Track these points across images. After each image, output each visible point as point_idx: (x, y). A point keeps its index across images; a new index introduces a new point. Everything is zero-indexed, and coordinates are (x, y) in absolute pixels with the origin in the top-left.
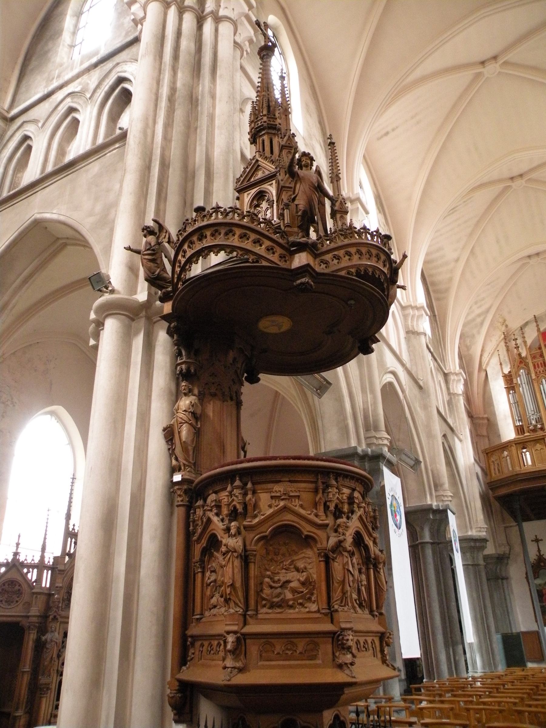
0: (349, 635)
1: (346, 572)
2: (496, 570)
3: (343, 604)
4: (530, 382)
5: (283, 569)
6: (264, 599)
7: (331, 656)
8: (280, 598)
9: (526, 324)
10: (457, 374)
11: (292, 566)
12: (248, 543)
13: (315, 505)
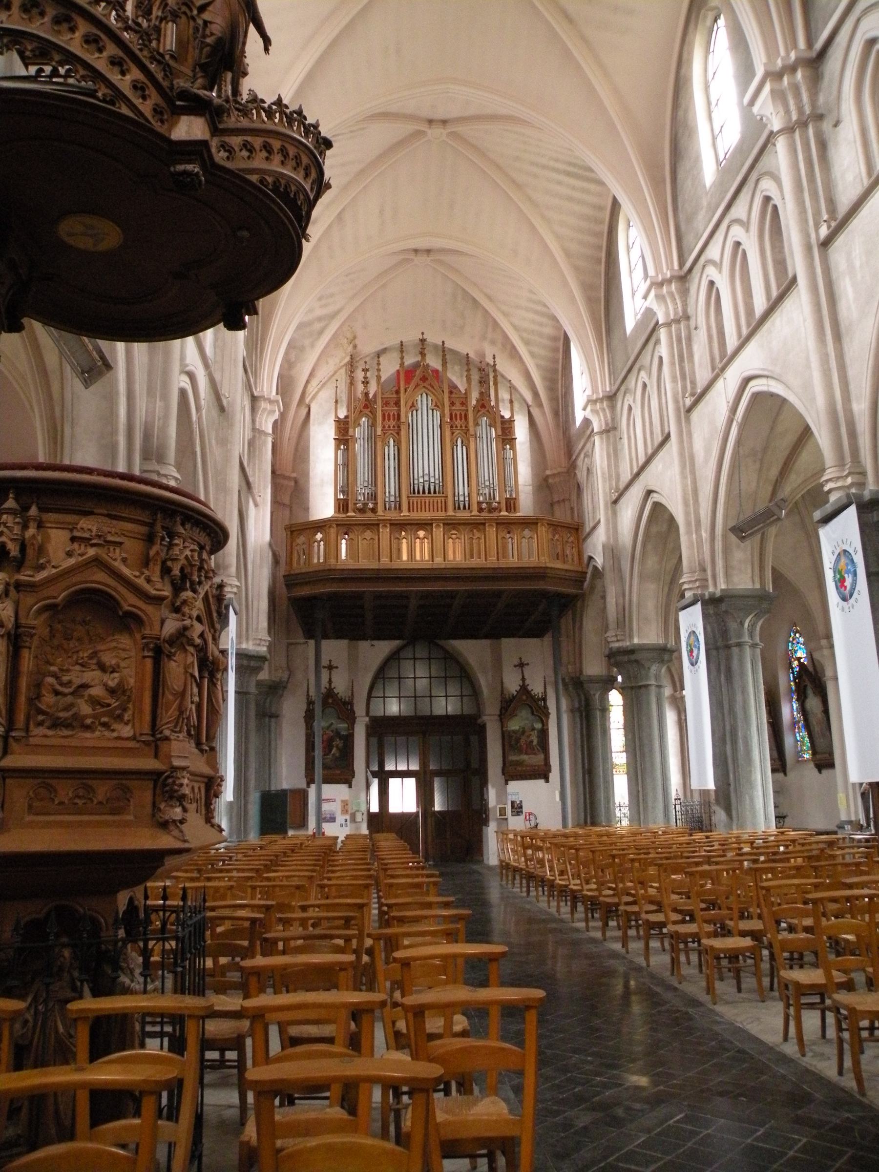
0: (184, 777)
1: (189, 678)
2: (264, 703)
3: (178, 729)
4: (372, 439)
5: (77, 663)
6: (41, 712)
7: (149, 809)
8: (70, 713)
9: (384, 351)
10: (271, 402)
11: (94, 661)
12: (22, 614)
13: (146, 562)
